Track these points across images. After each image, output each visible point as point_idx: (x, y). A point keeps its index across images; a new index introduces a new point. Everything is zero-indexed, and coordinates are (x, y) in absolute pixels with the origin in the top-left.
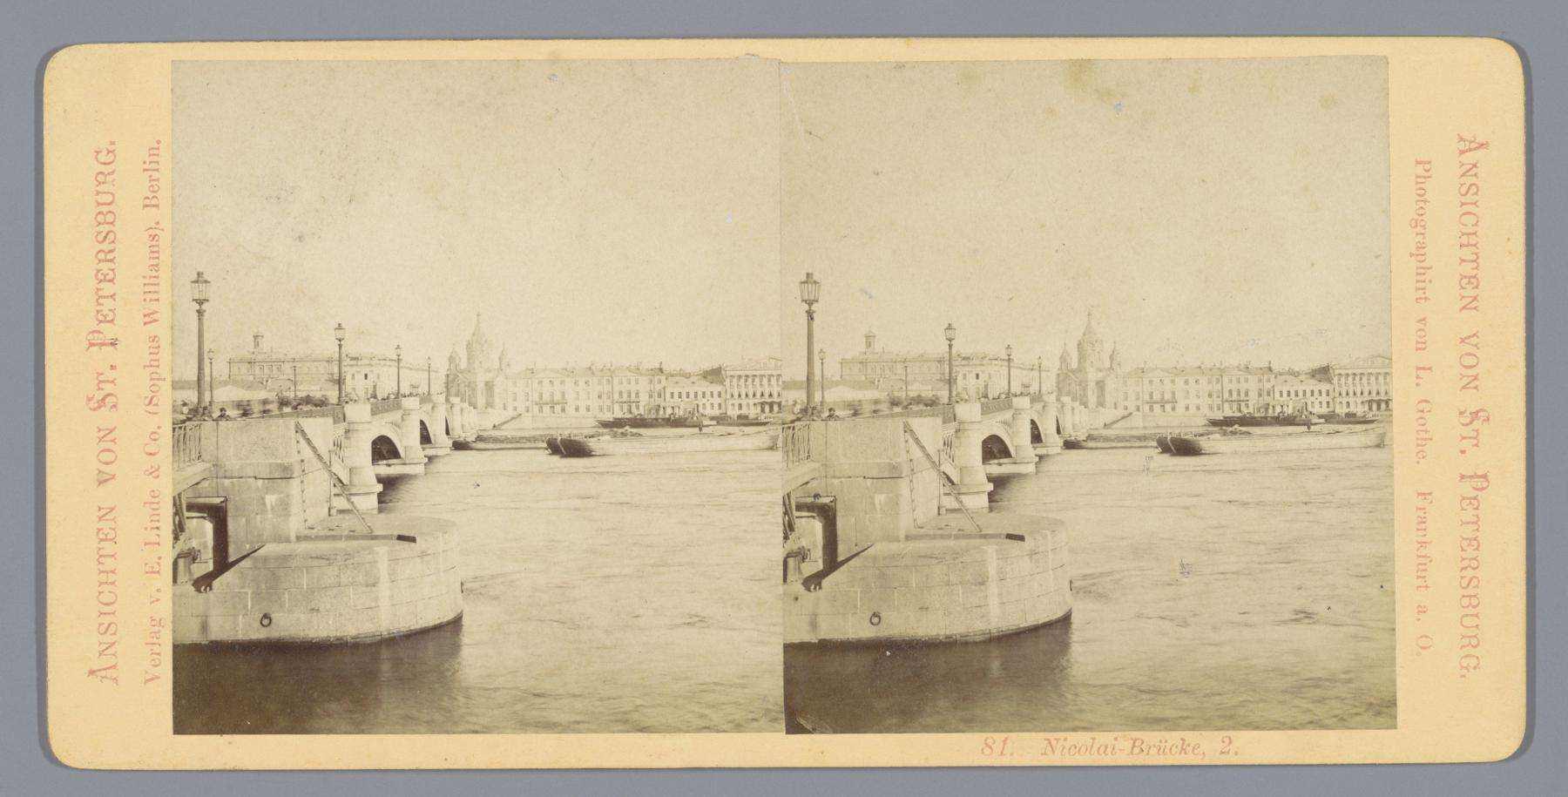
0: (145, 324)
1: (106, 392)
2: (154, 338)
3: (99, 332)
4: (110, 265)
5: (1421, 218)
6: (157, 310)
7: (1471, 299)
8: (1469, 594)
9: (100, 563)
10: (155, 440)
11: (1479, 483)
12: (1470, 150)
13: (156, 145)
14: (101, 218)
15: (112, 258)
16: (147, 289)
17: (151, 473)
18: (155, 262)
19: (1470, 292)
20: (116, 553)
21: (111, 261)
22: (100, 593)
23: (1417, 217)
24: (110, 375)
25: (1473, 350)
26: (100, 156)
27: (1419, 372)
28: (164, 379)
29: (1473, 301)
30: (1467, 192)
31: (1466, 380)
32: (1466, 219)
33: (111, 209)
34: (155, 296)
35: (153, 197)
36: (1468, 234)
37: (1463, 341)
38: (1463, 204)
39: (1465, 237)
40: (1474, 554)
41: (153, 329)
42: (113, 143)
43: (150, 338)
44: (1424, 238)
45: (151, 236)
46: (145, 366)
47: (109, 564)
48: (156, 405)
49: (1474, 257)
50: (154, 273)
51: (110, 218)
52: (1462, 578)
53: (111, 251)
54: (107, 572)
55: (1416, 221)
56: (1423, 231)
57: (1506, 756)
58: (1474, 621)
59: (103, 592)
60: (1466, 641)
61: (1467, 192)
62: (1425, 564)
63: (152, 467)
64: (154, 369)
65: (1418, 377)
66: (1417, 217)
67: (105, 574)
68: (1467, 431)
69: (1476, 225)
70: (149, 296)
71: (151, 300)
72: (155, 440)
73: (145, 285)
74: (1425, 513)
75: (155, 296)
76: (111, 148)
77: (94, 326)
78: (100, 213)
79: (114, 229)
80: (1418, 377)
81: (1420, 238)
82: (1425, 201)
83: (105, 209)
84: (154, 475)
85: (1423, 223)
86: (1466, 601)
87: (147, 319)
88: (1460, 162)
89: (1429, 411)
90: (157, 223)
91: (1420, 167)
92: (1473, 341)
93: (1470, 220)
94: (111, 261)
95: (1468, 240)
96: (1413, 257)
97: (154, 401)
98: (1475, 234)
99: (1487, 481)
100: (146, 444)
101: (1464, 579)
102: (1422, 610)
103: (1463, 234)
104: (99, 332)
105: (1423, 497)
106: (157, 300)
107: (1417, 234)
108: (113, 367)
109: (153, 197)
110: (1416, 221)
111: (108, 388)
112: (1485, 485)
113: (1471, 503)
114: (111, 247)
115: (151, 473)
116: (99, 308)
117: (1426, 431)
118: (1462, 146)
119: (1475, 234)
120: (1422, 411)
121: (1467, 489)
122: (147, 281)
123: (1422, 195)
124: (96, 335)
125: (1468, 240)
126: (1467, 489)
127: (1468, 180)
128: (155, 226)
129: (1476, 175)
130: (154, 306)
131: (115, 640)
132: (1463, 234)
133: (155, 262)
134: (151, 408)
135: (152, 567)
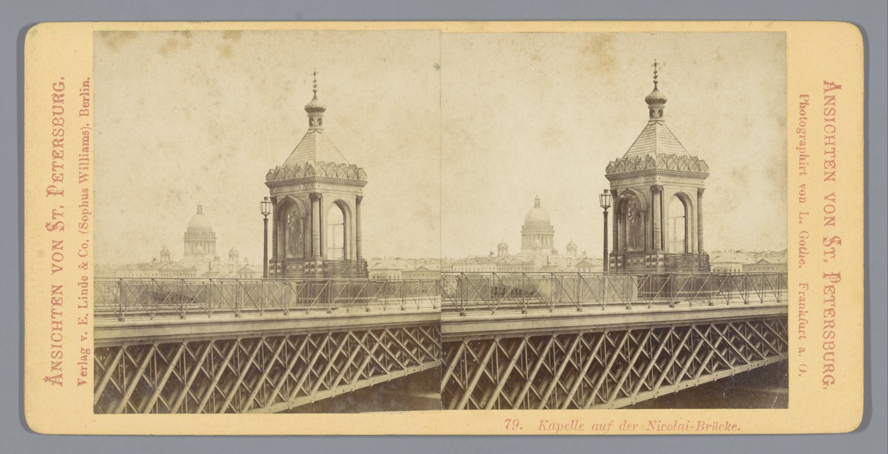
0: (80, 182)
1: (830, 247)
2: (86, 190)
3: (54, 187)
4: (827, 319)
5: (802, 128)
6: (87, 174)
7: (830, 174)
8: (59, 126)
9: (834, 148)
10: (85, 248)
11: (52, 190)
12: (831, 89)
13: (87, 80)
14: (832, 346)
15: (826, 323)
16: (82, 162)
17: (82, 267)
18: (86, 146)
19: (57, 296)
20: (62, 313)
21: (826, 322)
22: (834, 132)
23: (800, 127)
24: (59, 211)
25: (831, 203)
26: (832, 380)
27: (801, 215)
28: (90, 213)
29: (832, 175)
30: (830, 111)
31: (59, 246)
32: (58, 338)
33: (61, 117)
34: (86, 166)
35: (86, 110)
36: (829, 137)
37: (826, 198)
38: (826, 120)
39: (828, 139)
40: (56, 149)
41: (84, 185)
42: (63, 78)
43: (83, 189)
44: (804, 139)
45: (83, 132)
46: (80, 206)
47: (58, 318)
48: (86, 228)
49: (833, 150)
50: (86, 153)
51: (827, 346)
52: (825, 332)
53: (826, 327)
54: (830, 143)
55: (800, 129)
56: (804, 135)
57: (848, 430)
58: (56, 110)
59: (832, 132)
60: (827, 368)
61: (830, 111)
62: (804, 324)
63: (83, 263)
64: (86, 207)
65: (800, 218)
66: (800, 127)
67: (831, 142)
68: (59, 218)
69: (834, 132)
70: (82, 166)
71: (83, 168)
72: (85, 248)
73: (80, 160)
74: (804, 295)
75: (86, 166)
76: (62, 81)
77: (51, 183)
78: (56, 119)
79: (824, 340)
80: (800, 218)
81: (802, 139)
82: (805, 118)
83: (58, 116)
84: (84, 268)
85: (803, 131)
86: (61, 122)
87: (81, 179)
88: (62, 371)
89: (807, 238)
90: (88, 125)
91: (803, 98)
92: (55, 268)
93: (56, 337)
94: (826, 322)
95: (830, 140)
96: (798, 150)
97: (85, 226)
98: (833, 137)
99: (840, 277)
100: (80, 250)
101: (826, 333)
102: (802, 350)
103: (827, 137)
104: (54, 187)
105: (803, 286)
106: (87, 168)
107: (801, 136)
108: (62, 207)
109: (86, 110)
110: (800, 129)
111: (59, 218)
112: (838, 279)
113: (58, 178)
114: (826, 330)
115: (82, 267)
116: (54, 172)
117: (805, 248)
118: (60, 380)
119: (833, 137)
120: (803, 237)
121: (828, 282)
122: (81, 157)
123: (804, 115)
124: (52, 188)
125: (830, 140)
126: (828, 282)
127: (57, 360)
128: (86, 126)
129: (834, 104)
130: (85, 172)
131: (60, 361)
132: (827, 137)
133: (86, 146)
134: (83, 230)
135: (83, 320)
